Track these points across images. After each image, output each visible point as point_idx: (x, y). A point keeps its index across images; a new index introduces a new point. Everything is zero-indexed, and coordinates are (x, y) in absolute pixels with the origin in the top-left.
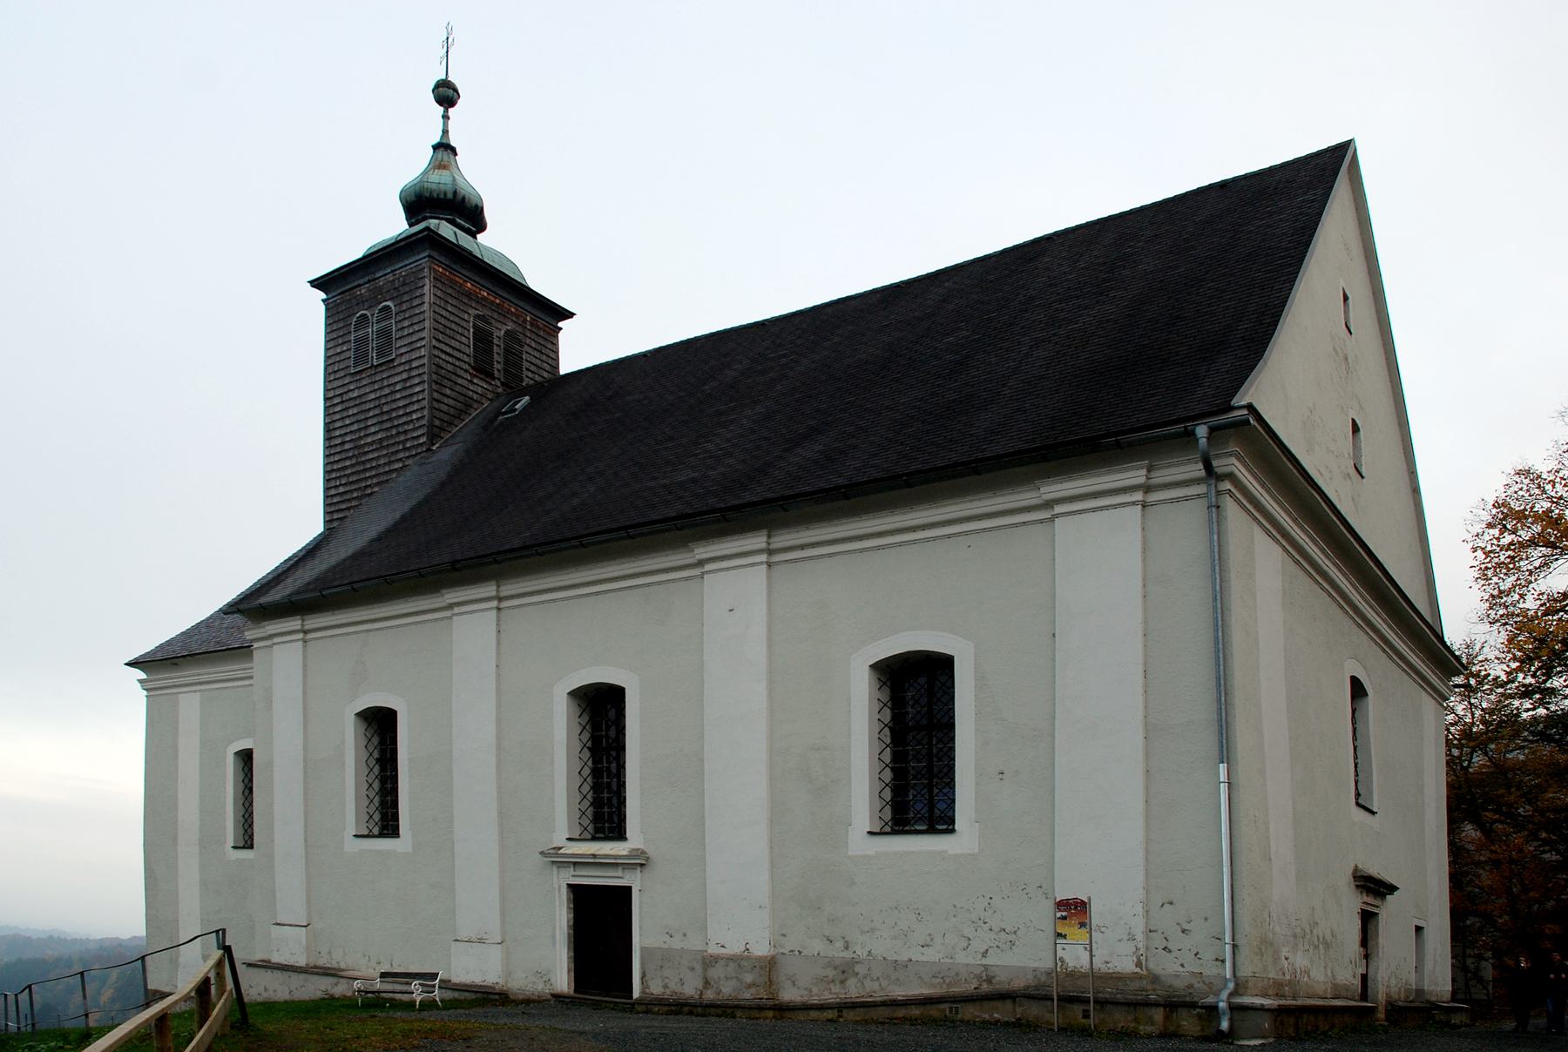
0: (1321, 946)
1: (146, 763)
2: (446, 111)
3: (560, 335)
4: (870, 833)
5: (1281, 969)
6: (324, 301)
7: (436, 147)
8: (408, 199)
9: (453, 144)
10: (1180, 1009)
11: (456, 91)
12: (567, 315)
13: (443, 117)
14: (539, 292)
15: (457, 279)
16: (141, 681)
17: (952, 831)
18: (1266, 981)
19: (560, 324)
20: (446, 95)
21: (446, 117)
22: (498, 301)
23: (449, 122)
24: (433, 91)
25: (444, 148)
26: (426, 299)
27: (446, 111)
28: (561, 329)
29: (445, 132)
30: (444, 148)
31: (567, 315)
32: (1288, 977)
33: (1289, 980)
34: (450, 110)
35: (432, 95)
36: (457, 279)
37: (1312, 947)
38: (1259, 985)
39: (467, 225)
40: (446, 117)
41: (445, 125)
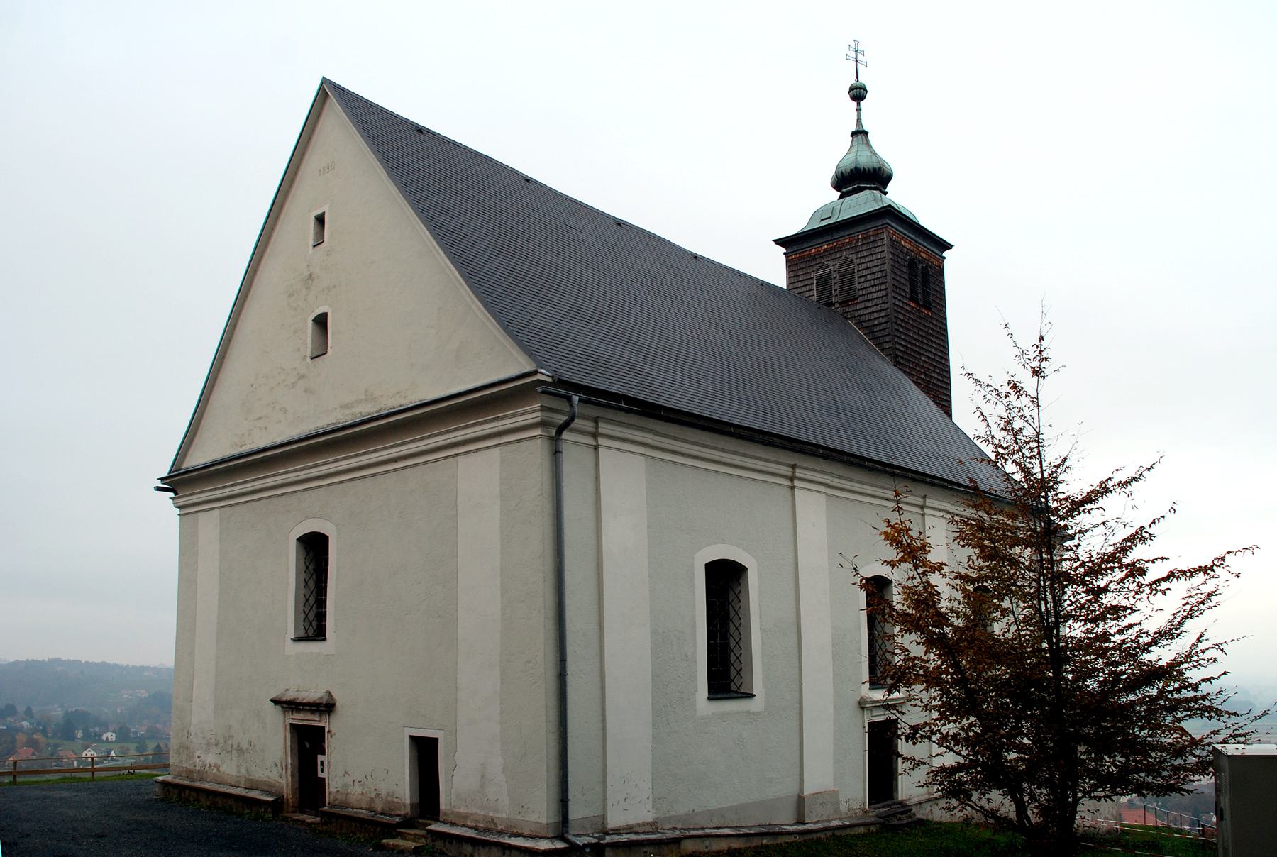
0: (234, 752)
2: (859, 104)
3: (945, 263)
5: (193, 763)
6: (784, 253)
7: (853, 134)
8: (844, 172)
10: (513, 851)
12: (949, 246)
14: (925, 227)
15: (805, 253)
16: (171, 498)
17: (325, 639)
18: (181, 769)
19: (944, 254)
20: (858, 94)
21: (859, 110)
22: (835, 244)
25: (860, 133)
27: (859, 104)
28: (944, 258)
29: (859, 120)
30: (860, 133)
31: (949, 246)
32: (198, 768)
33: (199, 771)
34: (861, 103)
36: (805, 253)
37: (224, 752)
38: (177, 770)
39: (851, 188)
40: (859, 110)
41: (859, 115)
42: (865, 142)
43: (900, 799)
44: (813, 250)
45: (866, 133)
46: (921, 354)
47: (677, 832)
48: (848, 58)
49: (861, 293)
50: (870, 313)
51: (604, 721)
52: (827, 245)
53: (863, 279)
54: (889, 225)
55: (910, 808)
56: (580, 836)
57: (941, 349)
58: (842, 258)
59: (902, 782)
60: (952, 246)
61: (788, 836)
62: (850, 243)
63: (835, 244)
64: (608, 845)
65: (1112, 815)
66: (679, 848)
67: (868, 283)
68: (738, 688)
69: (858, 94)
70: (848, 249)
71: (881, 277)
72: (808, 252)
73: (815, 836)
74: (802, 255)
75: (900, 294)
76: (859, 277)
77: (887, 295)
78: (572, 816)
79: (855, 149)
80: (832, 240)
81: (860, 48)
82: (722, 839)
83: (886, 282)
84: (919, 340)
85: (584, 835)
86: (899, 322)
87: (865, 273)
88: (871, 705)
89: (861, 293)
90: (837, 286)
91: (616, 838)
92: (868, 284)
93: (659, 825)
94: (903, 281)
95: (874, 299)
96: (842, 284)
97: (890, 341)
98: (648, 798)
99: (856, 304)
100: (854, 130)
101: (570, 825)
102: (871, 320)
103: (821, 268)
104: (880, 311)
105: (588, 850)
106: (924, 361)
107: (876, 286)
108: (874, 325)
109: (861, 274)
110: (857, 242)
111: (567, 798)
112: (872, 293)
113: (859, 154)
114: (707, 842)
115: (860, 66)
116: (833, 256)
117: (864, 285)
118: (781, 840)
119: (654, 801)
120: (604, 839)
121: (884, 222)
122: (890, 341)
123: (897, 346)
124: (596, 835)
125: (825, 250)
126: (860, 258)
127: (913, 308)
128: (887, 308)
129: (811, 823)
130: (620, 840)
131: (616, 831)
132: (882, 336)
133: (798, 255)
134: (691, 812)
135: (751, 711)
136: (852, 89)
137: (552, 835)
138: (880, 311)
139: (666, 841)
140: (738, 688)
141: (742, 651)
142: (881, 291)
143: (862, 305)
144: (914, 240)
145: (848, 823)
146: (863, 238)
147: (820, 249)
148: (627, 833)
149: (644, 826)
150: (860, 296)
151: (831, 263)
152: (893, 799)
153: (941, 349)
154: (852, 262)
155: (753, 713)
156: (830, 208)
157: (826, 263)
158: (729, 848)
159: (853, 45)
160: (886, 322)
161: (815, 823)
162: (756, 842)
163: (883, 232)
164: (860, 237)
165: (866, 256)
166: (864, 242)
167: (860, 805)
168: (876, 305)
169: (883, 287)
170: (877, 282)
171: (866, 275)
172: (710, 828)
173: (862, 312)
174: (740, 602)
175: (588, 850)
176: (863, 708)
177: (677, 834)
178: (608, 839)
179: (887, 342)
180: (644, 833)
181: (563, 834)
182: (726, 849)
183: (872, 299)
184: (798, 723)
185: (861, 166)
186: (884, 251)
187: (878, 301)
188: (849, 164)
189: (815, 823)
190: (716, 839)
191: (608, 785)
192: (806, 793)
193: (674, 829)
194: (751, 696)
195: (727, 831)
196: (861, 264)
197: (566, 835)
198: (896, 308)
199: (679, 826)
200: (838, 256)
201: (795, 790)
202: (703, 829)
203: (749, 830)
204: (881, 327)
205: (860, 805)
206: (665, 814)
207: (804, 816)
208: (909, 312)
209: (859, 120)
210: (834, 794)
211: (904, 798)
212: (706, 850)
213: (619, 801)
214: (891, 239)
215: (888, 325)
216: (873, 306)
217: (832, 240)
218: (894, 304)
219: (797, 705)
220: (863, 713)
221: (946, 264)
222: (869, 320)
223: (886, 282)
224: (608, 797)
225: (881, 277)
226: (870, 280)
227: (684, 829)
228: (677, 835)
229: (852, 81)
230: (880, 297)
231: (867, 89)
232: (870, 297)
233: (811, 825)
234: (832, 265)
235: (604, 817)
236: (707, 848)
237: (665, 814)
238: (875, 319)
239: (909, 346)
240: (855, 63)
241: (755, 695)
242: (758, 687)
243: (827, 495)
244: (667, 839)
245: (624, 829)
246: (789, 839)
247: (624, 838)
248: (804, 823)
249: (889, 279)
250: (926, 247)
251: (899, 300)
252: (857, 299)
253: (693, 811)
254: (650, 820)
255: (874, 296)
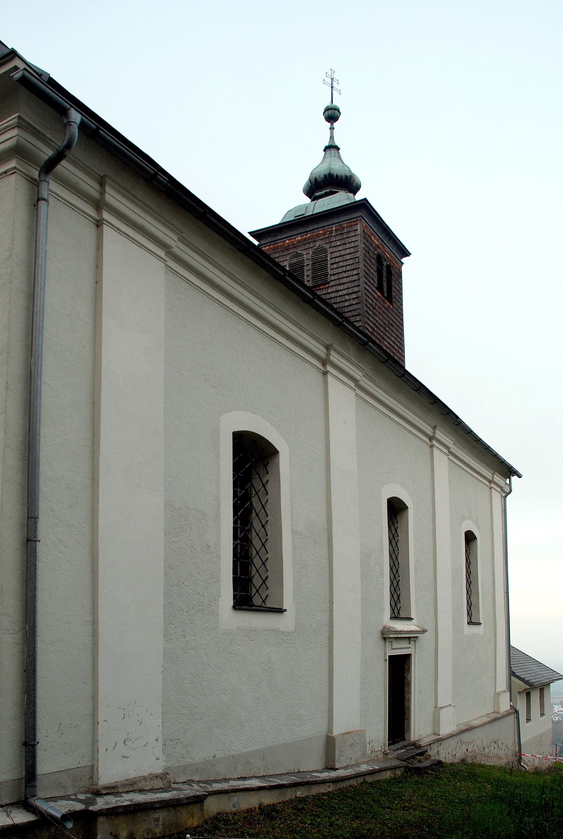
1: (408, 541)
4: (520, 476)
7: (327, 149)
8: (318, 179)
9: (336, 144)
11: (339, 111)
13: (330, 129)
15: (279, 244)
21: (332, 129)
22: (309, 235)
23: (334, 131)
24: (323, 114)
25: (332, 148)
26: (359, 232)
28: (403, 264)
29: (332, 137)
30: (332, 148)
35: (323, 117)
36: (279, 244)
40: (332, 129)
42: (337, 156)
43: (412, 739)
44: (287, 242)
45: (338, 149)
46: (384, 339)
47: (196, 787)
48: (325, 82)
49: (333, 278)
50: (342, 296)
51: (95, 623)
52: (301, 236)
53: (335, 266)
54: (364, 219)
55: (426, 748)
56: (54, 799)
57: (399, 340)
58: (315, 248)
59: (414, 721)
60: (410, 254)
61: (322, 786)
62: (324, 234)
63: (309, 235)
64: (101, 813)
65: (550, 753)
66: (202, 810)
67: (340, 269)
68: (264, 601)
69: (333, 113)
70: (323, 239)
71: (353, 264)
72: (282, 244)
73: (347, 783)
74: (276, 245)
75: (370, 281)
76: (332, 264)
77: (359, 279)
78: (42, 768)
79: (328, 160)
80: (306, 232)
81: (336, 77)
82: (252, 793)
83: (358, 268)
84: (383, 326)
85: (62, 798)
86: (368, 305)
87: (337, 260)
88: (394, 636)
89: (333, 278)
90: (309, 273)
91: (111, 801)
92: (340, 270)
93: (171, 777)
94: (372, 271)
95: (346, 283)
96: (314, 271)
97: (360, 320)
98: (157, 740)
99: (328, 288)
100: (327, 144)
101: (38, 783)
102: (342, 301)
103: (294, 257)
104: (352, 293)
105: (70, 825)
106: (386, 346)
107: (348, 271)
108: (344, 307)
109: (333, 261)
110: (331, 232)
111: (34, 739)
112: (344, 278)
113: (332, 163)
114: (235, 798)
115: (334, 91)
116: (307, 246)
117: (336, 271)
118: (315, 790)
119: (164, 745)
120: (94, 803)
121: (359, 215)
122: (360, 320)
123: (367, 325)
124: (82, 797)
125: (299, 241)
126: (333, 247)
127: (379, 297)
128: (359, 291)
129: (341, 768)
130: (120, 804)
131: (112, 790)
132: (352, 316)
133: (272, 246)
134: (211, 758)
135: (281, 629)
136: (327, 109)
137: (8, 801)
138: (352, 293)
139: (185, 801)
140: (264, 601)
141: (268, 556)
142: (352, 276)
143: (334, 289)
144: (381, 240)
145: (377, 768)
146: (337, 230)
147: (294, 240)
148: (127, 792)
149: (151, 780)
150: (331, 281)
151: (305, 253)
152: (404, 740)
153: (399, 340)
154: (325, 251)
155: (283, 633)
156: (307, 207)
157: (299, 252)
158: (260, 805)
159: (329, 73)
160: (357, 304)
161: (346, 768)
162: (290, 795)
163: (357, 224)
164: (334, 229)
165: (340, 245)
166: (338, 233)
167: (381, 747)
168: (348, 288)
169: (355, 272)
170: (349, 268)
171: (339, 262)
172: (234, 779)
173: (333, 295)
174: (267, 494)
175: (70, 825)
176: (385, 639)
177: (196, 790)
178: (101, 804)
179: (357, 321)
180: (152, 790)
181: (27, 798)
182: (257, 806)
183: (343, 284)
184: (327, 649)
185: (335, 172)
186: (358, 240)
187: (350, 285)
188: (324, 170)
189: (346, 768)
190: (246, 793)
191: (100, 719)
192: (336, 732)
193: (190, 782)
194: (280, 611)
195: (255, 783)
196: (334, 252)
197: (32, 800)
198: (366, 292)
199: (196, 778)
200: (311, 246)
201: (322, 730)
202: (226, 780)
203: (280, 780)
204: (352, 308)
205: (381, 747)
206: (473, 760)
207: (334, 761)
208: (376, 299)
209: (332, 137)
210: (361, 733)
211: (416, 739)
212: (234, 810)
213: (116, 744)
214: (364, 231)
215: (359, 306)
216: (345, 289)
217: (306, 232)
218: (365, 287)
219: (327, 629)
220: (385, 644)
221: (404, 268)
222: (339, 302)
223: (358, 268)
224: (100, 737)
225: (353, 264)
226: (343, 267)
227: (204, 782)
228: (198, 791)
229: (328, 103)
230: (352, 281)
231: (340, 111)
232: (342, 281)
233: (342, 771)
234: (305, 253)
235: (93, 769)
236: (234, 806)
237: (473, 760)
238: (346, 301)
239: (376, 329)
240: (330, 88)
241: (286, 610)
242: (288, 603)
243: (357, 395)
244: (187, 798)
245: (124, 785)
246: (323, 789)
247: (126, 800)
248: (335, 769)
249: (361, 265)
250: (389, 253)
251: (369, 286)
252: (329, 283)
253: (214, 757)
254: (159, 771)
255: (345, 280)
